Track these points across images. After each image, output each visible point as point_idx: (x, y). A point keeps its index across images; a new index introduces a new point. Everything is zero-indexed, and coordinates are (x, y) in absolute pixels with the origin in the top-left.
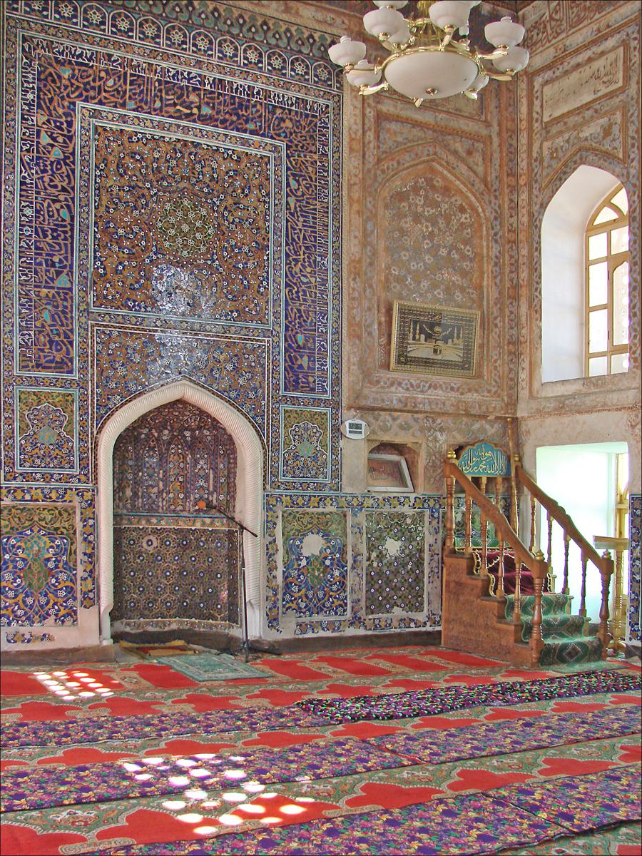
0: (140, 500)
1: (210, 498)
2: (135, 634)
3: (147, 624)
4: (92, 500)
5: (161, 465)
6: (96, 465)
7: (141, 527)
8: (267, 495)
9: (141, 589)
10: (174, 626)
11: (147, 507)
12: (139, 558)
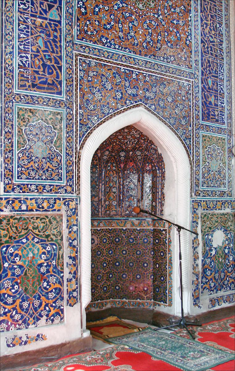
6: (79, 177)
10: (109, 306)
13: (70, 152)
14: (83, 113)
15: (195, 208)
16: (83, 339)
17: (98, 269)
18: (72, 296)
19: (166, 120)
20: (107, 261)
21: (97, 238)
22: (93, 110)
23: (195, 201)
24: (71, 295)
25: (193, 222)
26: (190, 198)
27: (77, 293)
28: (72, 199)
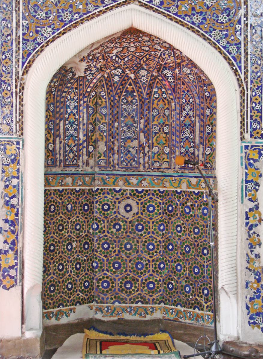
0: (116, 156)
1: (196, 153)
2: (108, 322)
3: (124, 310)
4: (16, 155)
5: (142, 113)
6: (21, 113)
7: (117, 189)
8: (246, 147)
9: (117, 265)
10: (158, 315)
11: (124, 164)
12: (114, 227)
13: (8, 78)
14: (27, 24)
15: (252, 159)
16: (24, 340)
17: (137, 252)
18: (8, 275)
19: (184, 19)
20: (156, 242)
21: (137, 203)
22: (45, 18)
23: (252, 146)
24: (6, 274)
25: (247, 182)
26: (240, 142)
27: (17, 271)
28: (10, 141)
